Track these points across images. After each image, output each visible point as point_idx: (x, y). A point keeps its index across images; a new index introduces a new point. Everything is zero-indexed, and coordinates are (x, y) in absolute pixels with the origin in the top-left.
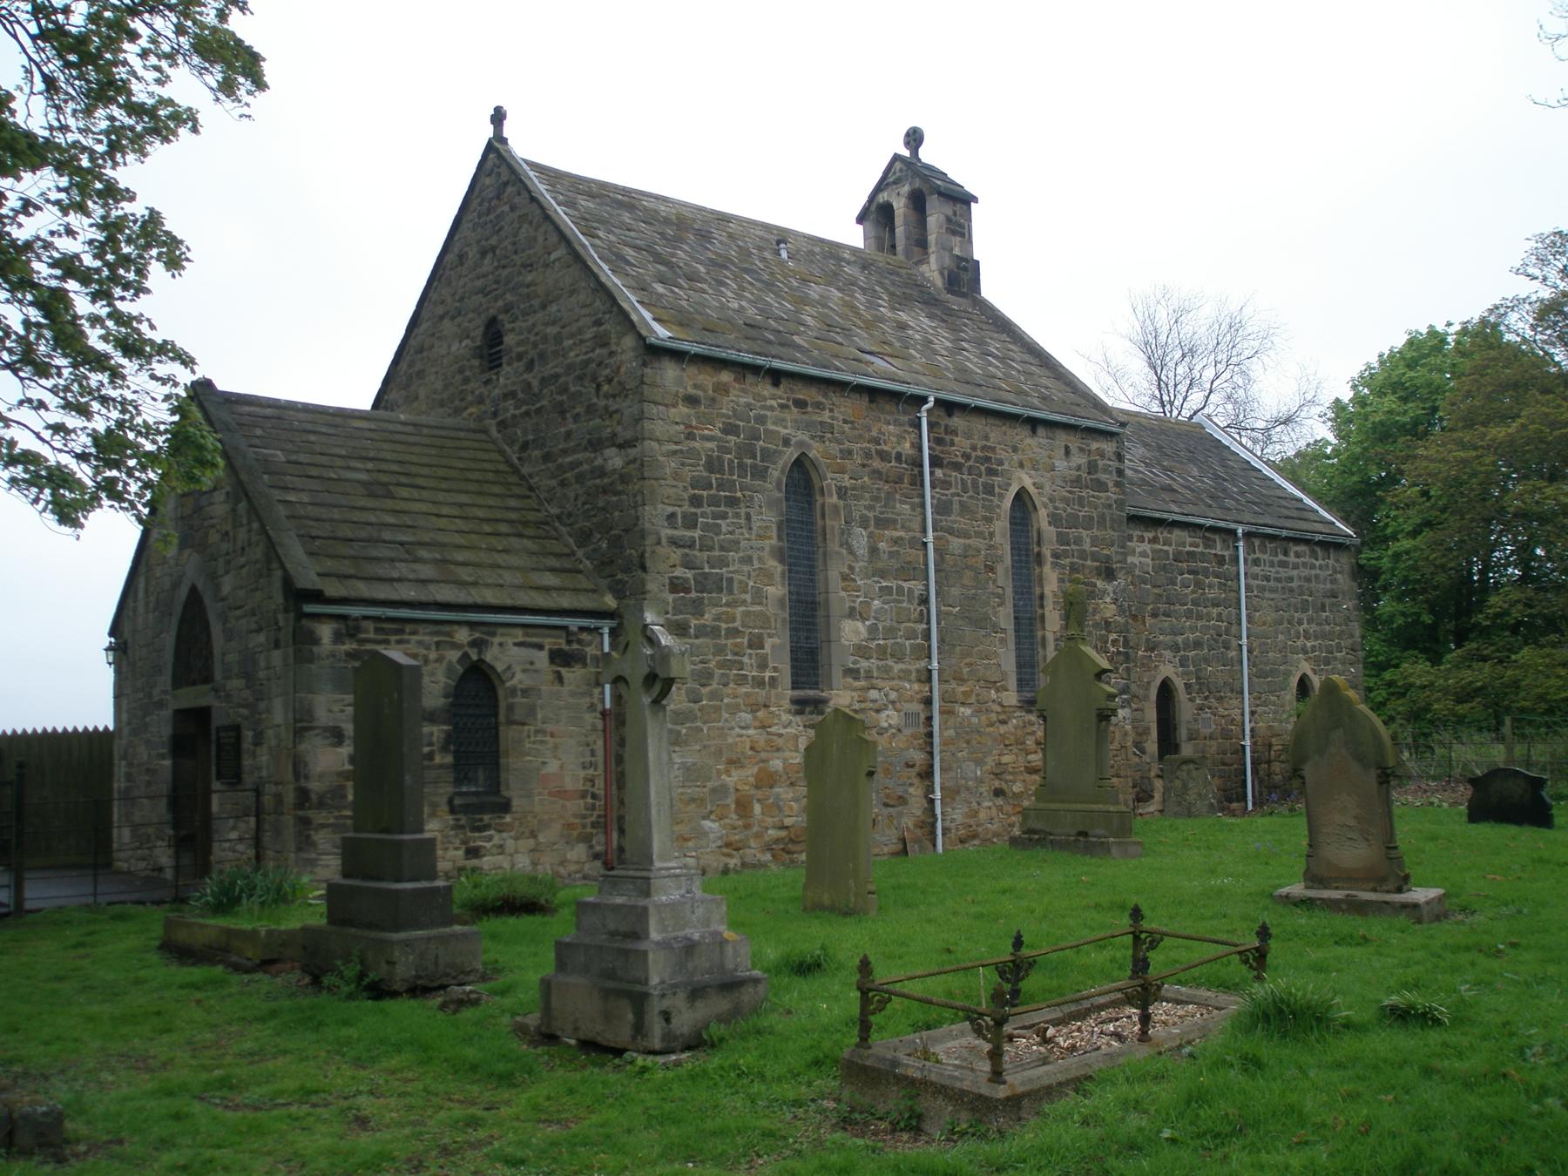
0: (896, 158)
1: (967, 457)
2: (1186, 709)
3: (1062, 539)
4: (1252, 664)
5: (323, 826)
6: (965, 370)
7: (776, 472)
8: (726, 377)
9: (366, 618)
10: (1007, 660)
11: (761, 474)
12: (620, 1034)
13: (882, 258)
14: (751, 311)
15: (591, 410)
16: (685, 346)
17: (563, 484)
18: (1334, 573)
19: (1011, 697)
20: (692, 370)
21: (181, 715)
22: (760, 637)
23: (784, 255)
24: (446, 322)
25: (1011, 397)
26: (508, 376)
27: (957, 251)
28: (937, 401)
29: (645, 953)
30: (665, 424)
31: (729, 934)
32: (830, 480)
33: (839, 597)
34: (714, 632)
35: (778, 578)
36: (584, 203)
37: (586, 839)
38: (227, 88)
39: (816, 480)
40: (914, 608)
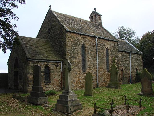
0: (93, 11)
1: (101, 44)
2: (124, 72)
3: (111, 53)
4: (131, 67)
5: (30, 84)
6: (101, 34)
7: (81, 45)
8: (75, 34)
9: (35, 61)
10: (106, 66)
11: (79, 45)
12: (65, 111)
13: (92, 22)
14: (78, 27)
15: (60, 38)
16: (71, 31)
17: (57, 46)
18: (140, 57)
19: (106, 71)
20: (71, 34)
21: (15, 72)
22: (79, 64)
23: (81, 21)
24: (44, 29)
25: (106, 37)
26: (51, 35)
27: (100, 21)
28: (98, 37)
29: (68, 102)
30: (68, 40)
31: (78, 99)
32: (86, 46)
33: (87, 59)
34: (74, 63)
35: (81, 57)
36: (59, 15)
37: (59, 86)
38: (21, 3)
39: (85, 46)
40: (95, 61)
